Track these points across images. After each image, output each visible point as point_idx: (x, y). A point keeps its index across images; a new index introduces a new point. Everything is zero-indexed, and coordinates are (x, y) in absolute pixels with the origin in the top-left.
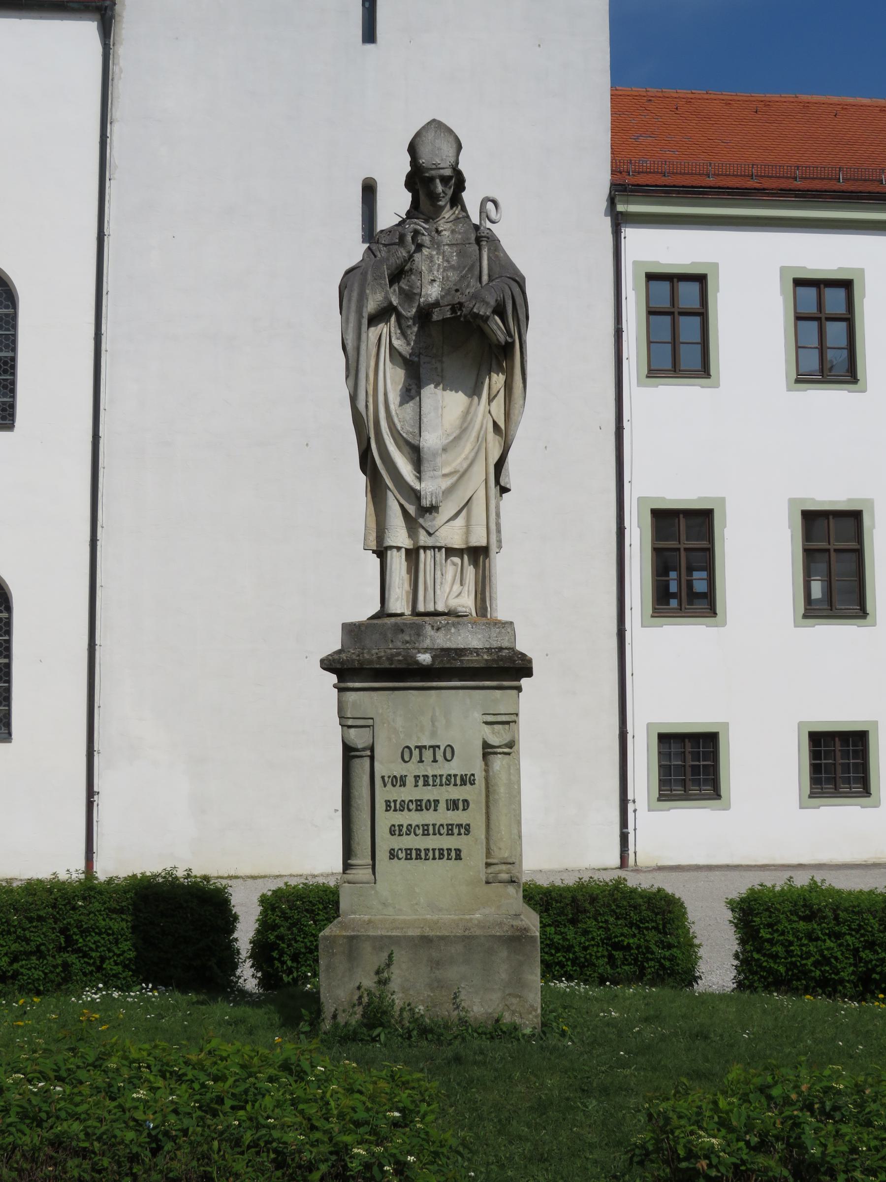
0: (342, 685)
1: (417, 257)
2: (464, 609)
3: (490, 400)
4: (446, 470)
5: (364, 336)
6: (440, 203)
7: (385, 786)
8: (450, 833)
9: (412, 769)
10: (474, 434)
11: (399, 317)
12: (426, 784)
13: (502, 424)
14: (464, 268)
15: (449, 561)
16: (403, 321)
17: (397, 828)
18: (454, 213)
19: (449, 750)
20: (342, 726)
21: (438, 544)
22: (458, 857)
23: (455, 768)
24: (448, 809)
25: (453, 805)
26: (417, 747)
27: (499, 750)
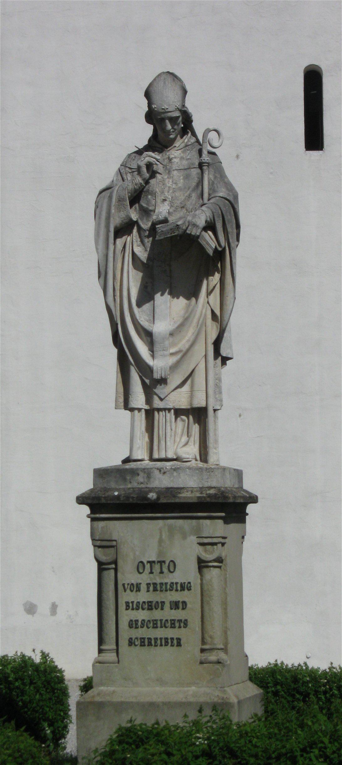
0: (93, 516)
1: (153, 181)
2: (188, 456)
3: (209, 293)
4: (172, 350)
5: (111, 247)
6: (172, 136)
7: (125, 591)
8: (173, 626)
9: (144, 578)
10: (195, 320)
11: (140, 229)
12: (155, 590)
13: (218, 312)
14: (189, 189)
15: (179, 419)
16: (142, 232)
17: (134, 622)
18: (183, 142)
19: (172, 564)
20: (95, 546)
21: (168, 407)
22: (179, 644)
23: (177, 577)
24: (171, 609)
25: (175, 605)
26: (148, 562)
27: (211, 564)
